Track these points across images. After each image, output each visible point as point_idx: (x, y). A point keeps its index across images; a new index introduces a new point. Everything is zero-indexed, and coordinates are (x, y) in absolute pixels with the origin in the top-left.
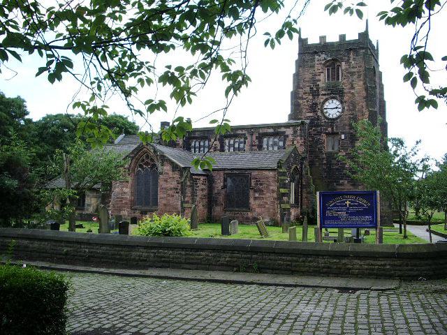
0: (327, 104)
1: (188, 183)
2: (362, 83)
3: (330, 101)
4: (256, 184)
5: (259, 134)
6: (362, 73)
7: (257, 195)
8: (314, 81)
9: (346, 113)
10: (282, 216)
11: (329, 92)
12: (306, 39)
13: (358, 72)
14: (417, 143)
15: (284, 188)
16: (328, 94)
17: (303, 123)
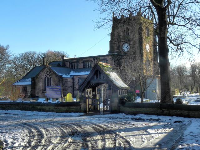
8: (119, 36)
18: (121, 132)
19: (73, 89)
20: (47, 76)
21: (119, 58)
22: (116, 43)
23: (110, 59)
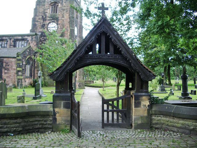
0: (50, 25)
2: (68, 15)
3: (52, 23)
4: (6, 66)
6: (68, 10)
7: (6, 71)
8: (45, 13)
9: (59, 30)
10: (18, 83)
11: (52, 19)
13: (66, 9)
15: (20, 67)
16: (51, 20)
17: (36, 34)
18: (131, 6)
19: (165, 115)
21: (43, 39)
22: (39, 20)
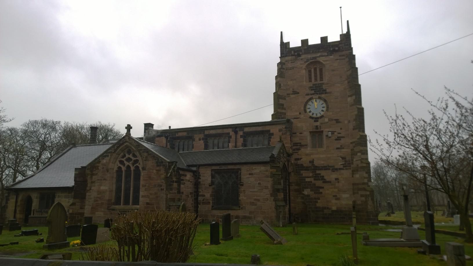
1: (175, 179)
5: (244, 133)
12: (288, 43)
14: (380, 135)
20: (127, 163)
23: (280, 130)
